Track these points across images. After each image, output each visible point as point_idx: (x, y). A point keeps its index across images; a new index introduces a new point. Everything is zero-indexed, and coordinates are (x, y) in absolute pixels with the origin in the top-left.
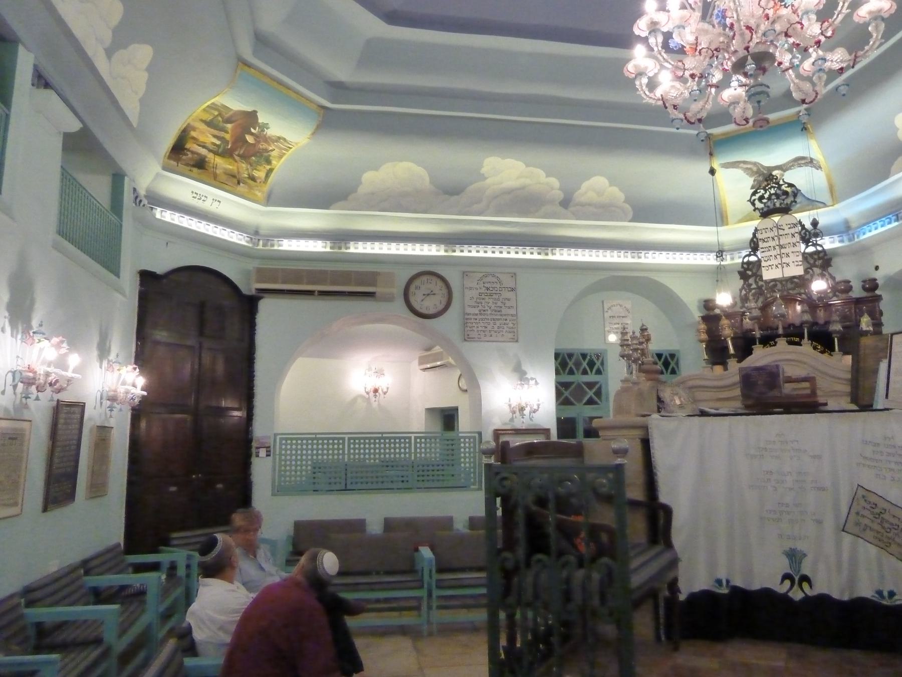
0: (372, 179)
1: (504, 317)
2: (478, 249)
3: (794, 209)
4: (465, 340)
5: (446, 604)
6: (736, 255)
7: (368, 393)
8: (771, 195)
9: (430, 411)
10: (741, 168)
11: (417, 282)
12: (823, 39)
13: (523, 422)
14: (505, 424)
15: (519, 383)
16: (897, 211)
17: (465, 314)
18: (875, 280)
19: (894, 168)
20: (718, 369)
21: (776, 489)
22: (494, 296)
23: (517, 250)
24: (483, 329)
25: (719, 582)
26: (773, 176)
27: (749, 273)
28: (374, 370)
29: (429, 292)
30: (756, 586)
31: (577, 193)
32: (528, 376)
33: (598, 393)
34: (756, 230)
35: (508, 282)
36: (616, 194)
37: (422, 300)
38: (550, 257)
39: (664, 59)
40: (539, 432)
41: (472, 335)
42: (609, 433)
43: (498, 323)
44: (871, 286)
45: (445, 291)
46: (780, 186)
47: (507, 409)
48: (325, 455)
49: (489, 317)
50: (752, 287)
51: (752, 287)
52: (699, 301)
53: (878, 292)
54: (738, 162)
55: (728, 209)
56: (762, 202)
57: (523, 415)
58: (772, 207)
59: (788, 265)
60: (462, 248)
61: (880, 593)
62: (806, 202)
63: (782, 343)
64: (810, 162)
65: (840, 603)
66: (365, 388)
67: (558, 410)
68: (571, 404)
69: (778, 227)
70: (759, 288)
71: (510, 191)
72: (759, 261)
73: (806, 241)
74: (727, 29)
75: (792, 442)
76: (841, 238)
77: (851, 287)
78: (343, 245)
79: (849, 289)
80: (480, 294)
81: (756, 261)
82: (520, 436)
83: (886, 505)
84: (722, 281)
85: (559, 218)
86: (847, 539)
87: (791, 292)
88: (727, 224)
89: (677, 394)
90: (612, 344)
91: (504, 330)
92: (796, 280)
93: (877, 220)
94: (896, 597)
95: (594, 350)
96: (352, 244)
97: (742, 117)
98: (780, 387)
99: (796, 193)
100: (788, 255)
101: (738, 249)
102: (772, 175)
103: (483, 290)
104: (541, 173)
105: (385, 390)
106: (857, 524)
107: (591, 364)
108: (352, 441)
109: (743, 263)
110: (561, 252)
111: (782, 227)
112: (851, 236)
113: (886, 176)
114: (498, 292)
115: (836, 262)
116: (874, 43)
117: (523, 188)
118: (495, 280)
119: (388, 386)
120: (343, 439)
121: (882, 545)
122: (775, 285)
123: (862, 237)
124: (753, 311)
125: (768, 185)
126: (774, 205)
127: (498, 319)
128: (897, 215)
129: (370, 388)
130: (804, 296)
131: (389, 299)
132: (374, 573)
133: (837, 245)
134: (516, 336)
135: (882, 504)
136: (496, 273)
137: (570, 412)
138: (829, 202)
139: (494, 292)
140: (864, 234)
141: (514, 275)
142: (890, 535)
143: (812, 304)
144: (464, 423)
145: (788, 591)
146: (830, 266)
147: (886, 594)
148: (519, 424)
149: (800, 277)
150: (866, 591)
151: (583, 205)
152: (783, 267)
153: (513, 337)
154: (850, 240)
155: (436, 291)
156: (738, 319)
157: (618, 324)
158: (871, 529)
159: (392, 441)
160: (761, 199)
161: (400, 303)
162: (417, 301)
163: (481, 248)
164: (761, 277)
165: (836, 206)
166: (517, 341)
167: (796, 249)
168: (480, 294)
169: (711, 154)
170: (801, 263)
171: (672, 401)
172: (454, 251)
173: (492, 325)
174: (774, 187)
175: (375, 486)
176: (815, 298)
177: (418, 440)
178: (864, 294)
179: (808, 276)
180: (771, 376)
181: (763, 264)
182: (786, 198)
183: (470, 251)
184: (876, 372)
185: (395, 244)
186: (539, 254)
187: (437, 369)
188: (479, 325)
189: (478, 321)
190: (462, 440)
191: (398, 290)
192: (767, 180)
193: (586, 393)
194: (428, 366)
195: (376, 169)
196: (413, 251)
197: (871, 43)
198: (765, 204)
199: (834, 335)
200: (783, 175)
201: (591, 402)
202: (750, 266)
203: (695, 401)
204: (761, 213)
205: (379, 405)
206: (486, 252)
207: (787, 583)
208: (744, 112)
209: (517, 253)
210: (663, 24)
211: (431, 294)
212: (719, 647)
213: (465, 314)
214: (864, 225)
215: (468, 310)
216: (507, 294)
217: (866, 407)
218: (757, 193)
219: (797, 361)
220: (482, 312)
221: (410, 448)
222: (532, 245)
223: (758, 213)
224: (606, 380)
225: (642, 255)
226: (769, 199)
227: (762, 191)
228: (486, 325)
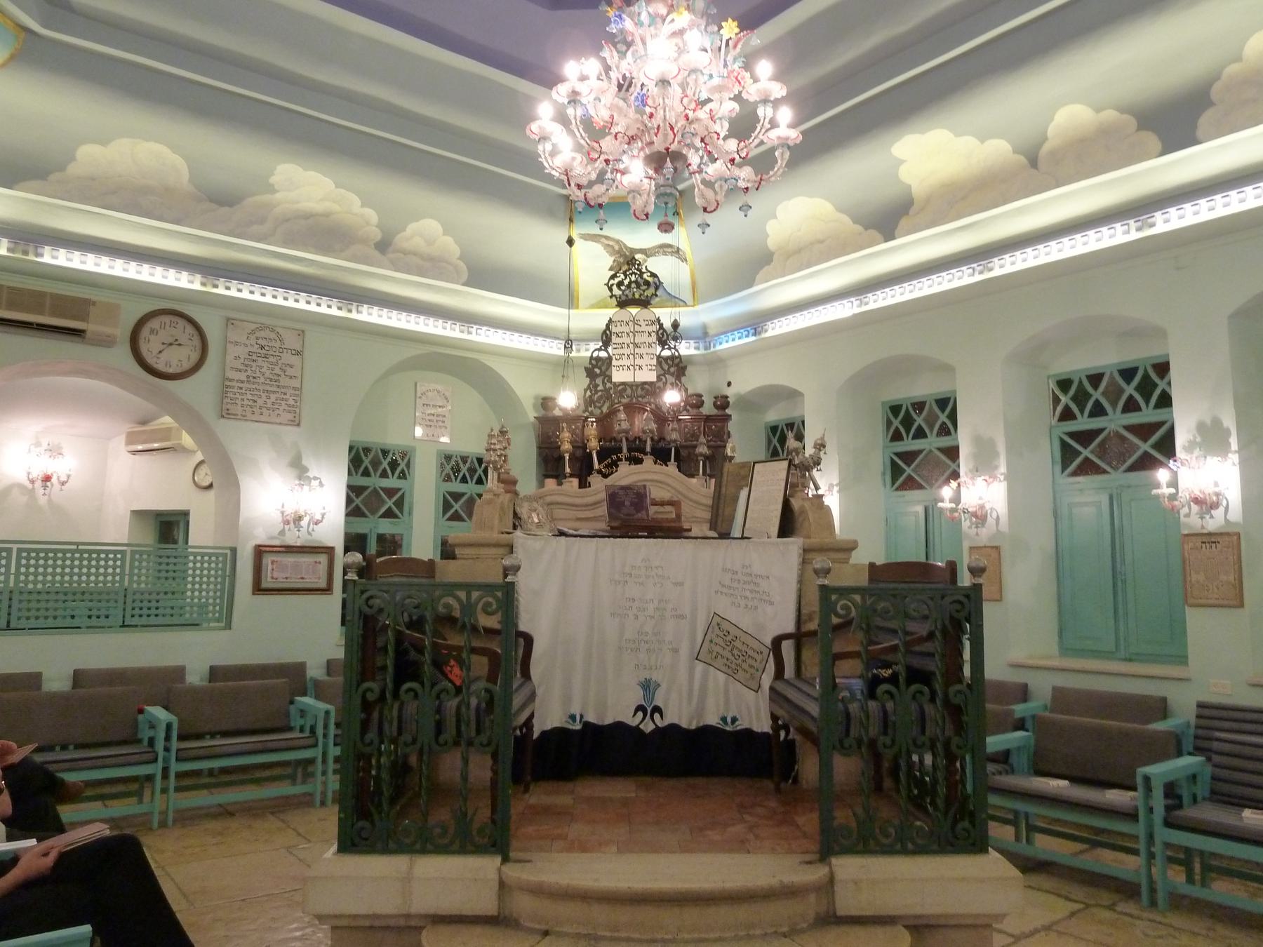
0: (90, 156)
1: (283, 390)
2: (252, 288)
3: (655, 301)
4: (222, 416)
5: (188, 781)
6: (583, 347)
7: (32, 482)
8: (631, 282)
9: (138, 514)
10: (602, 243)
11: (154, 324)
12: (737, 157)
13: (299, 537)
14: (272, 538)
15: (297, 482)
16: (754, 325)
17: (225, 379)
18: (727, 397)
19: (758, 277)
20: (551, 483)
21: (636, 617)
22: (271, 359)
23: (309, 299)
24: (251, 403)
25: (573, 717)
26: (636, 260)
27: (597, 371)
28: (45, 446)
29: (171, 340)
30: (608, 720)
31: (399, 236)
32: (310, 474)
33: (400, 503)
34: (610, 321)
35: (291, 341)
36: (449, 246)
37: (160, 352)
38: (354, 315)
39: (581, 136)
40: (319, 550)
41: (233, 409)
42: (467, 551)
43: (273, 397)
44: (722, 403)
45: (196, 341)
46: (642, 273)
47: (278, 518)
48: (68, 567)
49: (261, 387)
50: (599, 389)
51: (599, 389)
52: (536, 398)
53: (728, 411)
54: (599, 235)
55: (580, 289)
56: (620, 289)
57: (299, 527)
58: (630, 296)
59: (641, 368)
60: (228, 284)
61: (724, 719)
62: (665, 297)
63: (648, 461)
64: (677, 252)
65: (687, 731)
66: (29, 473)
67: (347, 523)
68: (363, 515)
69: (635, 322)
70: (607, 390)
71: (308, 216)
72: (610, 358)
73: (663, 343)
74: (645, 117)
75: (657, 568)
76: (697, 344)
77: (703, 402)
78: (31, 249)
79: (700, 404)
80: (250, 354)
81: (607, 358)
82: (293, 555)
83: (738, 633)
84: (568, 377)
85: (372, 265)
86: (700, 667)
87: (640, 399)
88: (577, 307)
89: (535, 511)
90: (420, 440)
91: (281, 408)
92: (646, 386)
93: (734, 331)
94: (737, 723)
95: (398, 445)
96: (47, 250)
97: (643, 211)
98: (647, 510)
99: (658, 286)
100: (641, 357)
101: (587, 340)
102: (634, 258)
103: (255, 349)
104: (356, 201)
105: (63, 478)
106: (710, 652)
107: (394, 465)
108: (24, 554)
109: (591, 357)
110: (370, 310)
111: (639, 323)
112: (708, 344)
113: (750, 285)
114: (277, 354)
115: (689, 371)
116: (778, 169)
117: (327, 215)
118: (273, 335)
119: (71, 473)
120: (9, 551)
121: (730, 672)
122: (625, 390)
123: (719, 348)
124: (623, 423)
125: (630, 269)
126: (634, 295)
127: (274, 392)
128: (755, 329)
129: (37, 473)
130: (653, 406)
131: (106, 342)
132: (71, 747)
133: (692, 352)
134: (297, 417)
135: (733, 631)
136: (236, 320)
137: (362, 526)
138: (690, 302)
139: (271, 353)
140: (721, 344)
141: (302, 333)
142: (737, 662)
143: (661, 417)
144: (201, 534)
145: (640, 724)
146: (684, 375)
147: (729, 720)
148: (293, 538)
149: (651, 384)
150: (712, 720)
151: (406, 253)
152: (635, 370)
153: (293, 419)
154: (706, 348)
155: (183, 339)
156: (580, 425)
157: (433, 415)
158: (722, 657)
159: (42, 555)
160: (620, 284)
161: (126, 348)
162: (150, 348)
163: (257, 288)
164: (610, 377)
165: (697, 308)
166: (298, 425)
167: (650, 351)
168: (250, 354)
169: (571, 220)
170: (654, 368)
171: (529, 517)
172: (216, 286)
173: (264, 398)
174: (635, 274)
175: (41, 623)
176: (665, 410)
177: (137, 556)
178: (714, 412)
179: (660, 384)
180: (638, 496)
181: (614, 362)
182: (647, 289)
183: (240, 290)
184: (735, 499)
185: (122, 261)
186: (340, 308)
187: (154, 453)
188: (244, 397)
189: (243, 391)
190: (191, 558)
191: (122, 331)
192: (628, 264)
193: (383, 502)
194: (140, 447)
195: (104, 142)
196: (151, 277)
197: (776, 169)
198: (623, 291)
199: (699, 458)
200: (645, 261)
201: (389, 514)
202: (600, 363)
203: (553, 520)
204: (618, 302)
205: (50, 501)
206: (263, 295)
207: (640, 714)
208: (645, 206)
209: (308, 303)
210: (585, 95)
211: (176, 343)
212: (570, 785)
213: (225, 379)
214: (722, 334)
215: (230, 374)
216: (288, 358)
217: (725, 536)
218: (617, 277)
219: (661, 482)
220: (252, 379)
221: (122, 567)
222: (330, 295)
223: (614, 301)
224: (412, 486)
225: (474, 330)
226: (629, 286)
227: (622, 276)
228: (255, 398)
